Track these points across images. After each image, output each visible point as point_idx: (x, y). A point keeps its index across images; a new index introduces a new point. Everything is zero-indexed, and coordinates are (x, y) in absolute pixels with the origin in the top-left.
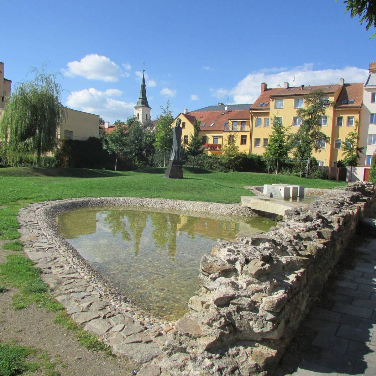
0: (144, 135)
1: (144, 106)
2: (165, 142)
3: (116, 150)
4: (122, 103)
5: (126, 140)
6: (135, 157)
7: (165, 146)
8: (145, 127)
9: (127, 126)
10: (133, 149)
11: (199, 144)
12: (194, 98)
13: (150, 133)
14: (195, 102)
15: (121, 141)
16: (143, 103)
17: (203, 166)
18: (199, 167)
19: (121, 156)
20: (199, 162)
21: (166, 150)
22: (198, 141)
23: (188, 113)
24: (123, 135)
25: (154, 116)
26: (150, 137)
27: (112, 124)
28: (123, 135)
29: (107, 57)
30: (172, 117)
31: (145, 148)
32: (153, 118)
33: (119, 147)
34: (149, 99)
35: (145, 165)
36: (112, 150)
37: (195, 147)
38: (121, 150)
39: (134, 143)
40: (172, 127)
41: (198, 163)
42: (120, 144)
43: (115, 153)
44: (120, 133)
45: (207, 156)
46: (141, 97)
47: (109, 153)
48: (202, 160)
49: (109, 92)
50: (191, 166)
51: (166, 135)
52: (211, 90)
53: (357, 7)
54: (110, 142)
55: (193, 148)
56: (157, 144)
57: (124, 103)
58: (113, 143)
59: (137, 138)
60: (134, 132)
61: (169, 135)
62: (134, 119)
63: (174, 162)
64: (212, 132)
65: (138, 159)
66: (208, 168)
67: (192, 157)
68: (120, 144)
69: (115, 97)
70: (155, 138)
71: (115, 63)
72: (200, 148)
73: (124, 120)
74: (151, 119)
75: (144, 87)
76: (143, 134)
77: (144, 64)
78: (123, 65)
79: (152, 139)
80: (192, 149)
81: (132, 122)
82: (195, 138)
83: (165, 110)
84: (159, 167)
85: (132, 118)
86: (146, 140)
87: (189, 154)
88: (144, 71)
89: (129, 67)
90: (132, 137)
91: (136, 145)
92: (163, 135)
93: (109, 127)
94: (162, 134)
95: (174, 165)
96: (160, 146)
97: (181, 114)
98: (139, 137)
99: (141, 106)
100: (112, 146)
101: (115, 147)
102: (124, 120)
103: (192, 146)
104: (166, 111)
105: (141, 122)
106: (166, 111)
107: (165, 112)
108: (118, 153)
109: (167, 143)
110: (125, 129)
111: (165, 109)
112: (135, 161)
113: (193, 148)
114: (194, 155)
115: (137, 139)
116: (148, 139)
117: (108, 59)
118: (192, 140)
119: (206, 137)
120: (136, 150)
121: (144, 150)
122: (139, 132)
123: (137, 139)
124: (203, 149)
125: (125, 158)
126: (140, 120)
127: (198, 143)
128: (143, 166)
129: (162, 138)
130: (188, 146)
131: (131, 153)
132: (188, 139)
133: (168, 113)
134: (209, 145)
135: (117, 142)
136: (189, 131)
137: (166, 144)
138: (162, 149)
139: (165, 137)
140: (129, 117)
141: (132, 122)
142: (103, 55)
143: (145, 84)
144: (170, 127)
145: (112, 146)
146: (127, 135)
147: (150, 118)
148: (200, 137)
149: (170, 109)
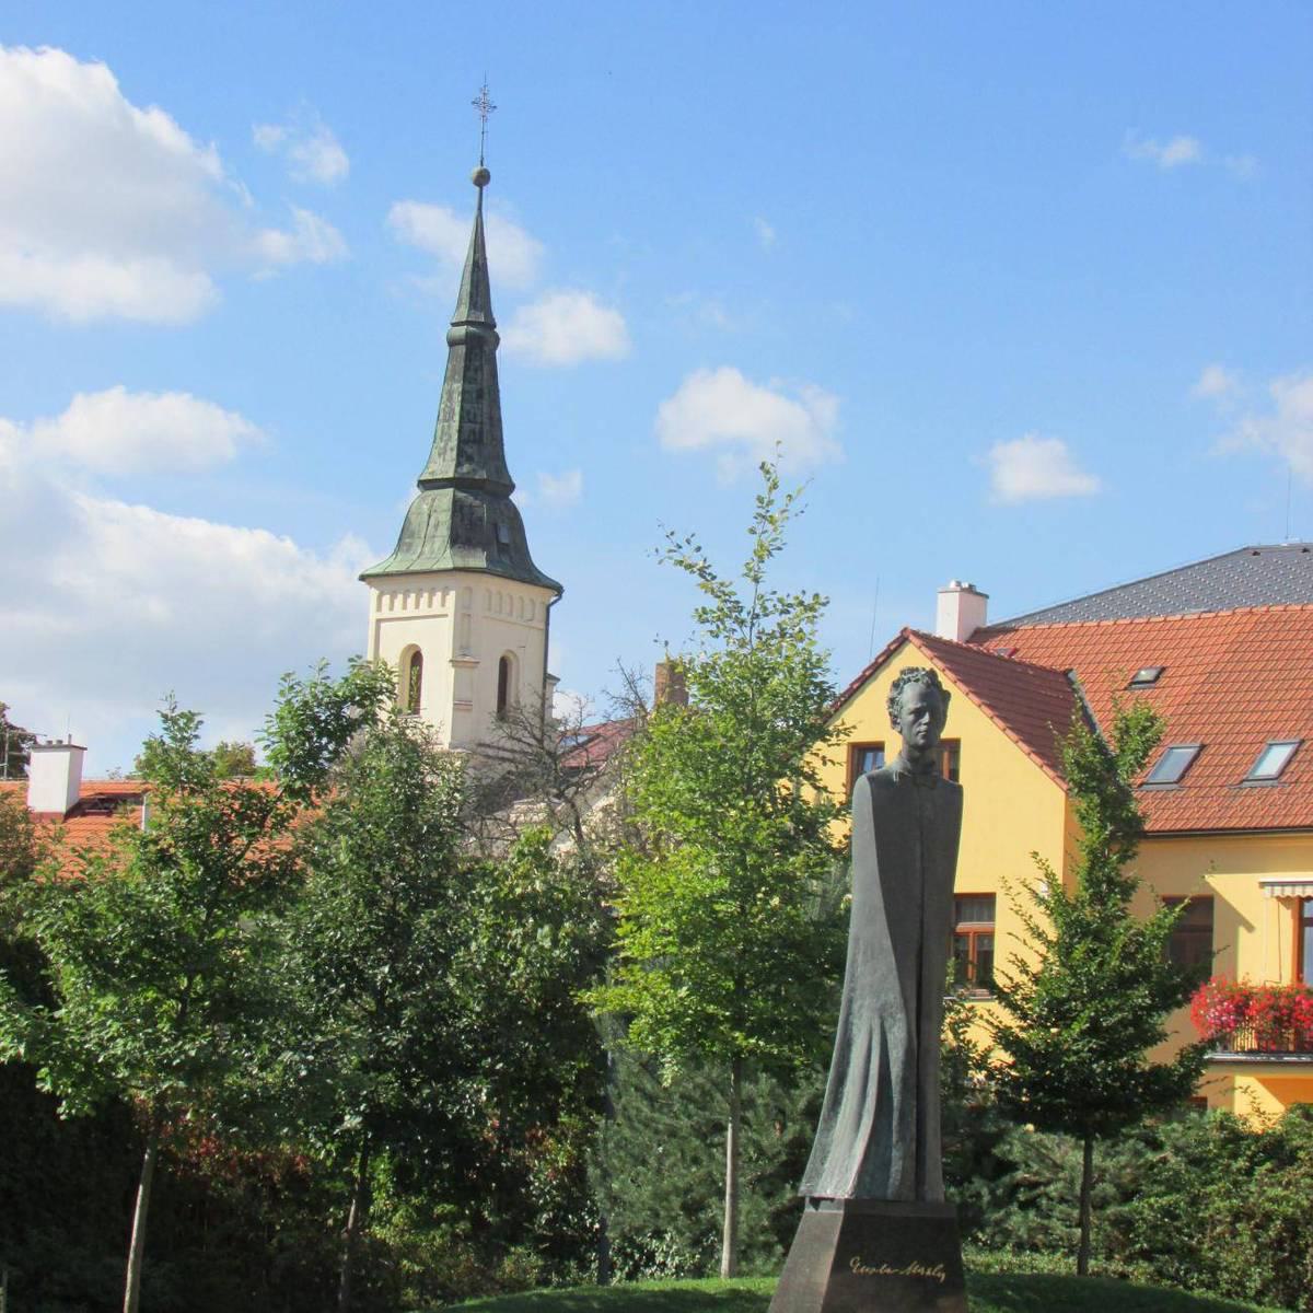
0: (480, 889)
1: (479, 560)
2: (726, 966)
3: (135, 1065)
4: (244, 545)
5: (265, 946)
6: (371, 1150)
7: (737, 1022)
8: (492, 799)
9: (273, 787)
10: (348, 1063)
11: (1141, 996)
12: (1026, 469)
13: (547, 865)
14: (1045, 515)
15: (201, 958)
16: (464, 532)
17: (1191, 1253)
18: (1140, 1274)
19: (208, 1150)
20: (1146, 1207)
21: (740, 1064)
22: (1127, 957)
23: (981, 634)
24: (222, 887)
25: (594, 671)
26: (548, 910)
27: (114, 760)
28: (222, 887)
29: (82, 53)
30: (811, 666)
31: (486, 1038)
32: (581, 698)
33: (181, 1025)
34: (536, 497)
35: (491, 1243)
36: (91, 1072)
37: (1094, 1030)
38: (193, 1070)
39: (359, 981)
40: (808, 793)
41: (1125, 1224)
42: (182, 997)
43: (129, 1110)
44: (190, 871)
45: (1234, 1138)
46: (446, 468)
47: (53, 1100)
48: (1174, 1185)
49: (99, 424)
50: (1045, 1263)
51: (745, 890)
52: (1214, 380)
53: (282, 981)
54: (69, 978)
55: (1073, 1037)
56: (638, 998)
57: (263, 537)
58: (103, 986)
59: (390, 921)
60: (358, 853)
61: (788, 878)
62: (367, 694)
63: (866, 1226)
64: (1277, 844)
65: (404, 1182)
66: (1254, 1284)
67: (1067, 1152)
68: (182, 997)
69: (164, 483)
70: (610, 922)
71: (183, 121)
72: (1151, 1038)
73: (241, 726)
74: (562, 706)
75: (476, 351)
76: (467, 880)
77: (485, 106)
78: (267, 136)
79: (576, 941)
80: (1053, 1054)
81: (324, 728)
82: (1089, 914)
83: (721, 593)
84: (652, 1282)
85: (336, 683)
86: (494, 953)
87: (1021, 1115)
88: (482, 179)
89: (330, 161)
90: (330, 903)
91: (386, 1015)
92: (708, 887)
93: (78, 809)
94: (695, 871)
95: (856, 1266)
96: (676, 1018)
97: (902, 641)
98: (414, 909)
99: (447, 563)
100: (90, 1015)
101: (132, 1032)
102: (241, 726)
103: (1059, 1013)
104: (748, 602)
105: (443, 740)
106: (745, 594)
107: (732, 610)
108: (164, 1111)
109: (773, 985)
110: (256, 813)
111: (729, 570)
112: (365, 1199)
113: (1073, 1037)
114: (1084, 1131)
115: (394, 933)
116: (529, 937)
117: (101, 76)
118: (1064, 950)
119: (1205, 904)
120: (378, 1067)
121: (470, 1072)
122: (416, 850)
123: (394, 933)
124: (1194, 1060)
125: (251, 1171)
126: (438, 717)
127: (1125, 982)
128: (467, 1257)
129: (698, 924)
130: (1007, 1018)
131: (317, 1102)
132: (988, 937)
133: (769, 624)
134: (1242, 1004)
135: (153, 976)
136: (1014, 829)
137: (741, 991)
138: (694, 1061)
139: (725, 908)
140: (306, 676)
141: (342, 731)
142: (34, 44)
143: (490, 325)
144: (784, 785)
145: (90, 1015)
146: (275, 887)
147: (545, 703)
148: (1144, 914)
149: (782, 579)
